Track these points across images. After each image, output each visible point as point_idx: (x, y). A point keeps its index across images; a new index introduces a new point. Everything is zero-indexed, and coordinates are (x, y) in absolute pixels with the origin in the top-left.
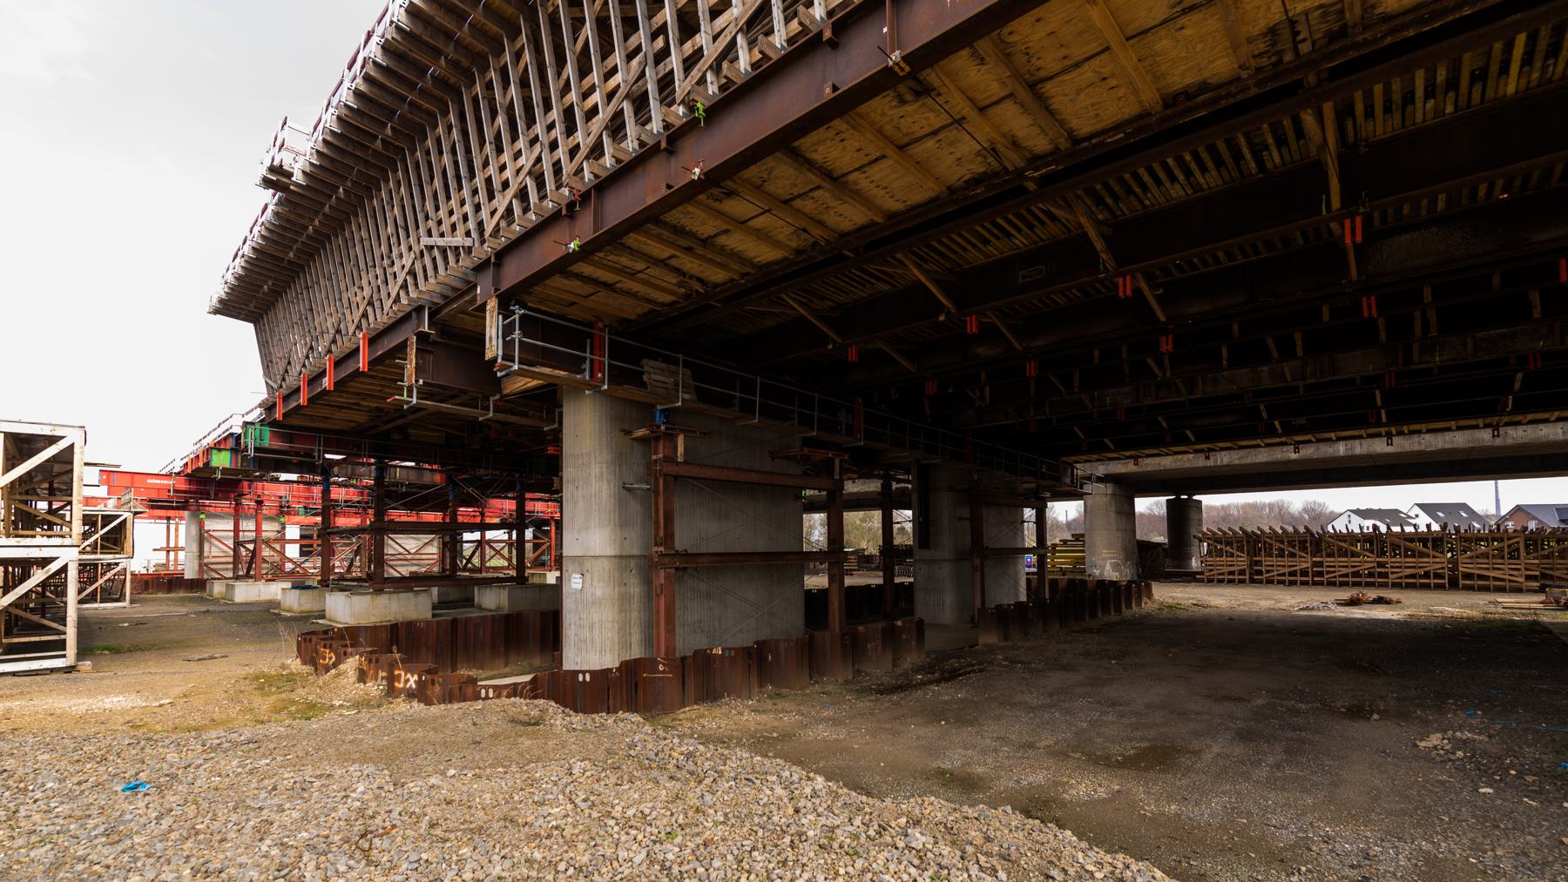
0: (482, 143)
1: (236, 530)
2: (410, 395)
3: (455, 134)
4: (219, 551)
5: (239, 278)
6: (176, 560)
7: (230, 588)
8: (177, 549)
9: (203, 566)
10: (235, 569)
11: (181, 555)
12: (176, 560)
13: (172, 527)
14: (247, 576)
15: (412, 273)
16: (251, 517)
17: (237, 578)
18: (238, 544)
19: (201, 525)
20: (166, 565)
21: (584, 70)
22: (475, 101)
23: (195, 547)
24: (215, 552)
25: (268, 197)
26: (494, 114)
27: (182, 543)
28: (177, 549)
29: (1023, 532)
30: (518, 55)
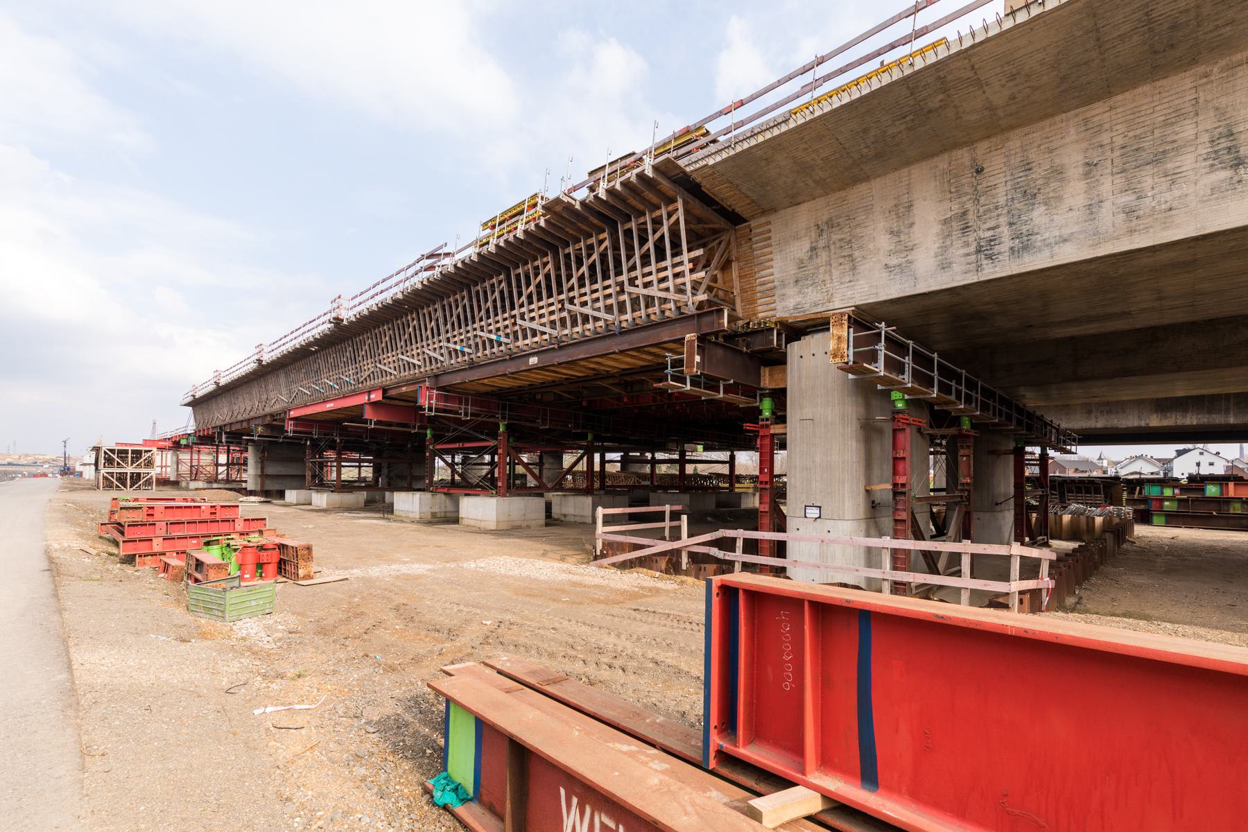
0: (426, 330)
1: (191, 459)
2: (371, 424)
3: (466, 301)
4: (184, 469)
5: (278, 358)
6: (166, 472)
7: (188, 483)
8: (166, 466)
9: (178, 475)
10: (191, 477)
11: (169, 469)
12: (166, 472)
13: (164, 456)
14: (195, 480)
15: (369, 376)
16: (262, 484)
17: (191, 480)
18: (192, 466)
19: (178, 456)
20: (161, 474)
21: (645, 260)
22: (424, 315)
23: (175, 466)
24: (184, 469)
25: (215, 386)
26: (431, 321)
27: (169, 464)
28: (166, 466)
29: (1190, 623)
30: (463, 298)
